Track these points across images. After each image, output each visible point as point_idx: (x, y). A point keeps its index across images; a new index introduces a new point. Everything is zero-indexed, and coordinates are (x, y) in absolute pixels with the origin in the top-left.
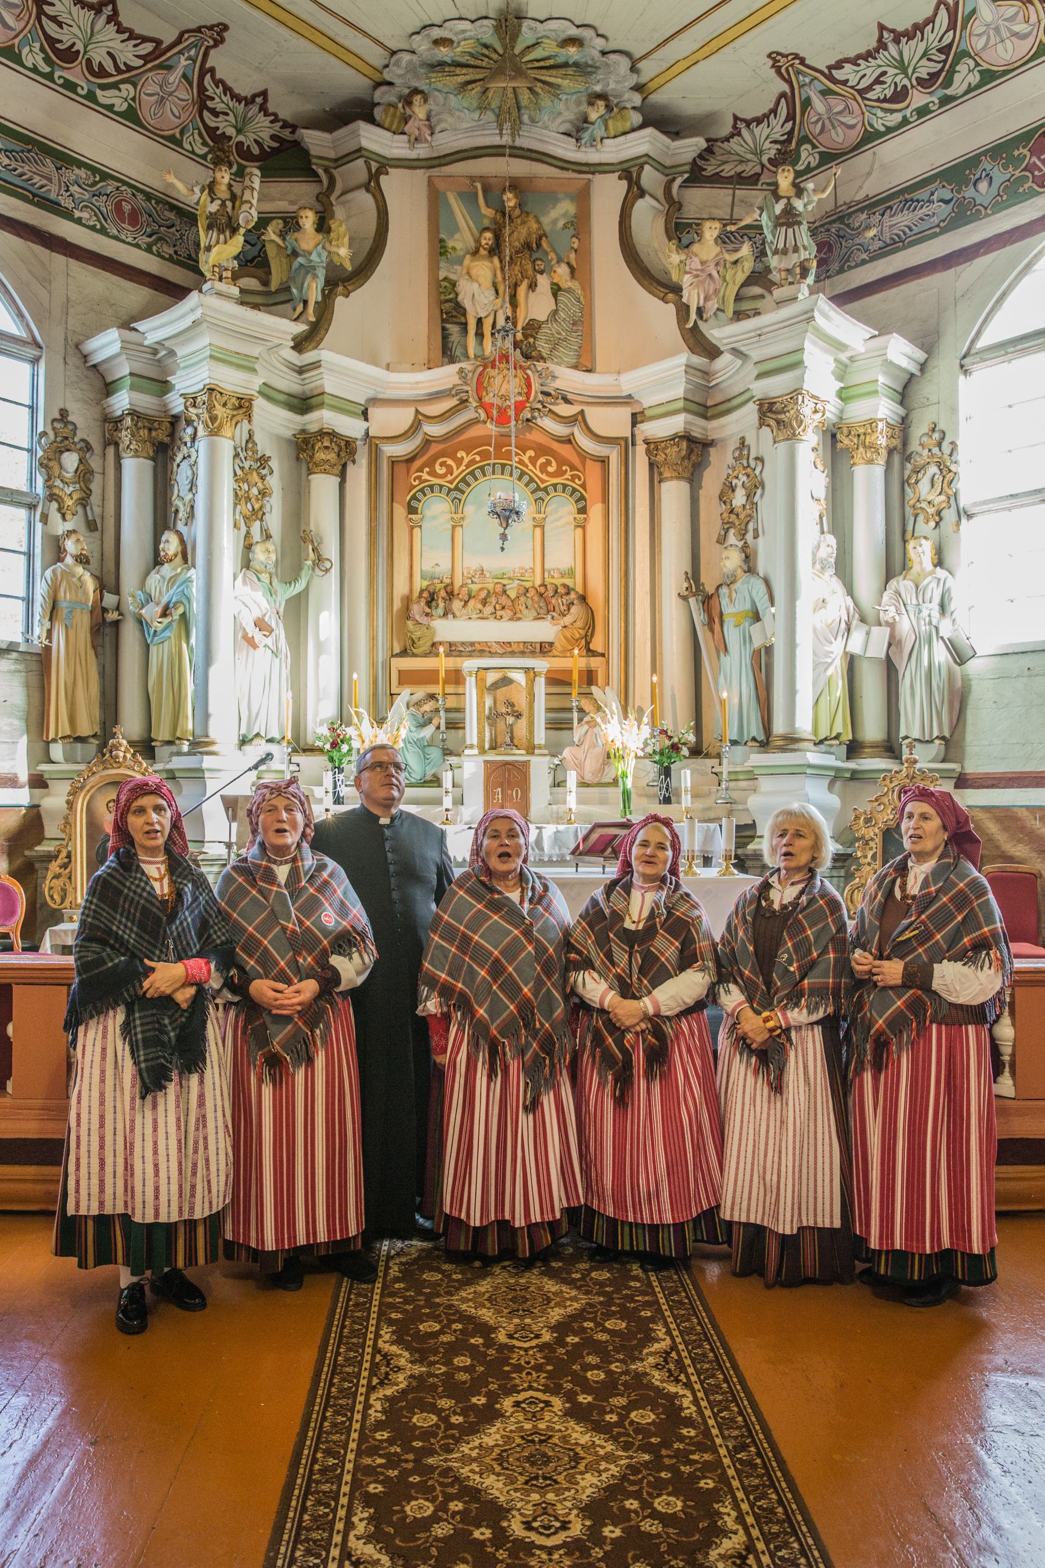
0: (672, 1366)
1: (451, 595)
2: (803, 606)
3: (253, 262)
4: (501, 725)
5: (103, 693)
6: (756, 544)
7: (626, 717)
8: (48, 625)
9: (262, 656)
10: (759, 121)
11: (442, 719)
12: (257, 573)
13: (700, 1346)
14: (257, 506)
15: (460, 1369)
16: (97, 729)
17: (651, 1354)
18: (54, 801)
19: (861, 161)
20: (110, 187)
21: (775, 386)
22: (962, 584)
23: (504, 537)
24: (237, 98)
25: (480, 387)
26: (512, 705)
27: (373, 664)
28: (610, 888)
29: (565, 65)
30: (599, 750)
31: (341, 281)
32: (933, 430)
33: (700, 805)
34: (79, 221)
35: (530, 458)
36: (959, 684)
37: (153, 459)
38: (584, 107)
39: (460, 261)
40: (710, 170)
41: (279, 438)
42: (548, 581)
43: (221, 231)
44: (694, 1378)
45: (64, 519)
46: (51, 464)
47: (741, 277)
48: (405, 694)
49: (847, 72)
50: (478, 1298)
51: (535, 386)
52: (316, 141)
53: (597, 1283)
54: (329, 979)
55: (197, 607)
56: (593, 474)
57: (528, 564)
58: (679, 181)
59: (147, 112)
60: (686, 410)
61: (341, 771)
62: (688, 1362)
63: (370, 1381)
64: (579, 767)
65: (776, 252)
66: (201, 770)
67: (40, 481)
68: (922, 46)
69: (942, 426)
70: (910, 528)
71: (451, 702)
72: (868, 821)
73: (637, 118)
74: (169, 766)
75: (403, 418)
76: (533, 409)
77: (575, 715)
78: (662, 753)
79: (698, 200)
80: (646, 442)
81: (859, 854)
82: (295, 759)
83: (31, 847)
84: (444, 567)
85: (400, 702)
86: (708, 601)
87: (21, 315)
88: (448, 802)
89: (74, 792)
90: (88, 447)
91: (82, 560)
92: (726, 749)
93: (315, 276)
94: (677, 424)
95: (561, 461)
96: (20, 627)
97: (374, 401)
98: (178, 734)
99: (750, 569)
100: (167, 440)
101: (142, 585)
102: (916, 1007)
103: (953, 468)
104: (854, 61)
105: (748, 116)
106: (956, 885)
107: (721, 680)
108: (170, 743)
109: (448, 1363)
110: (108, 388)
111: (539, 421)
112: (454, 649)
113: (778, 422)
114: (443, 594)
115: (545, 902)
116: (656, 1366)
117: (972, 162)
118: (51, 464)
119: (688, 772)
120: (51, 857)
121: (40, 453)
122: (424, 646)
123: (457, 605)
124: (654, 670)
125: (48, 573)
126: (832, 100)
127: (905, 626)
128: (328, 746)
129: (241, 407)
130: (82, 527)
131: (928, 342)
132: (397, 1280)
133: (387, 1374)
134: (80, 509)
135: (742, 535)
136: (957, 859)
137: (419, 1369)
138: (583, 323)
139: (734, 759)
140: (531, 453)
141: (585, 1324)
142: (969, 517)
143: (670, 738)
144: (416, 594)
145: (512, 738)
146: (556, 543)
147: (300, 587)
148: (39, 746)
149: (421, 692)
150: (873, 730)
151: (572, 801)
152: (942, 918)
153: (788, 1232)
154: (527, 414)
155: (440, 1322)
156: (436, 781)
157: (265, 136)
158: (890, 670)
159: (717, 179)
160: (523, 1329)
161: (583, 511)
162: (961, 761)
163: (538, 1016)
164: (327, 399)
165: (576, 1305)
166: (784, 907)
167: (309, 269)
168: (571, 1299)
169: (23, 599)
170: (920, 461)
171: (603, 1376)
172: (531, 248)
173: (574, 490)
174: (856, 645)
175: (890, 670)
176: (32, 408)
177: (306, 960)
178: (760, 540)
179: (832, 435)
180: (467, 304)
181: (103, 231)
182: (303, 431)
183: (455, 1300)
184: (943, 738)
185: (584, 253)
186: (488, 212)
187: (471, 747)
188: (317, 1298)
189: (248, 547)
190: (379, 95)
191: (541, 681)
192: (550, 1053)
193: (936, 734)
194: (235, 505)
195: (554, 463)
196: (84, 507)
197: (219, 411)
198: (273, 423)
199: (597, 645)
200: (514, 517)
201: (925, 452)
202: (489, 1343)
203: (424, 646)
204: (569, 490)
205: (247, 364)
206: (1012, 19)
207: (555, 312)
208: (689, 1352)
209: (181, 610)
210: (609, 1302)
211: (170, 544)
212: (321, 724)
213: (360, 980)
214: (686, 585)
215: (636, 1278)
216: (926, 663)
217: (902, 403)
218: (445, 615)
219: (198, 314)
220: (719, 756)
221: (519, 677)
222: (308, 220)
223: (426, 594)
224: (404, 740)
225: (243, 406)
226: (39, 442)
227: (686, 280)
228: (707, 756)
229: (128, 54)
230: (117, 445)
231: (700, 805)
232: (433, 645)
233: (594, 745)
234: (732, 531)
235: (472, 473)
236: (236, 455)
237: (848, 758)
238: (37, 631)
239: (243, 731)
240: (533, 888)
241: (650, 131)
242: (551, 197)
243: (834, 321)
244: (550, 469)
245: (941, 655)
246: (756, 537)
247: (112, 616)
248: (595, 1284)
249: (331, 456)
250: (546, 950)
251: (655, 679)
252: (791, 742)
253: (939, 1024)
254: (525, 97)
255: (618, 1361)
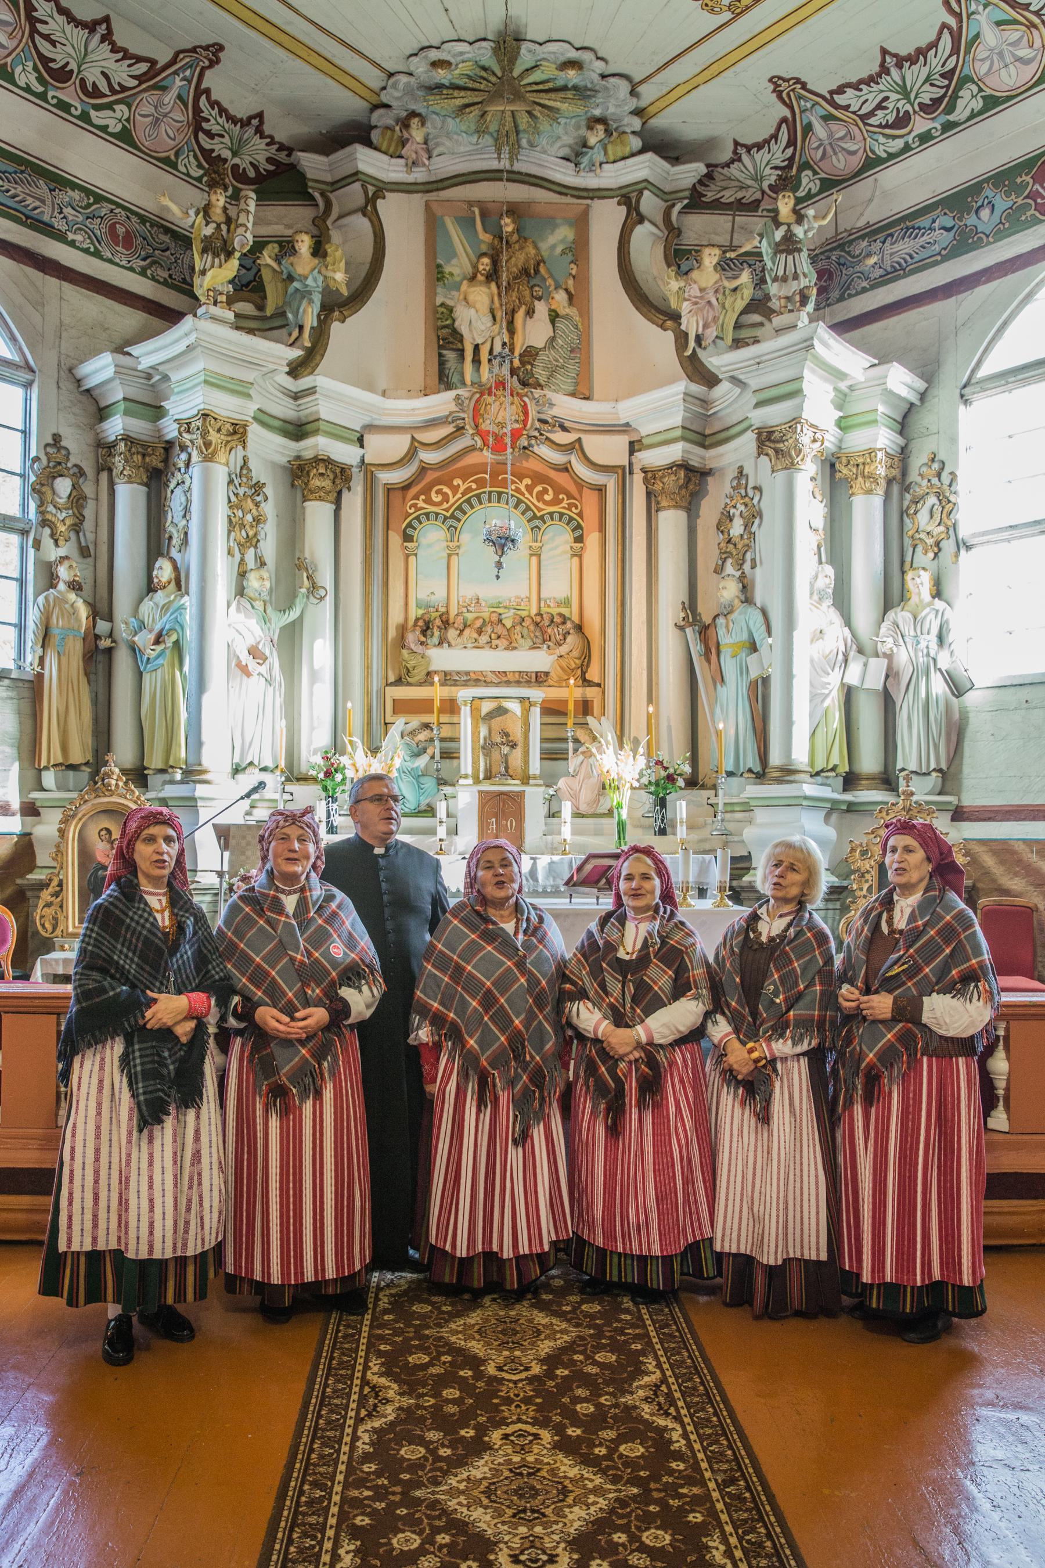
0: (662, 1399)
1: (446, 624)
2: (800, 637)
3: (249, 286)
4: (496, 755)
5: (96, 720)
6: (754, 575)
7: (621, 747)
8: (40, 652)
9: (255, 685)
10: (759, 146)
11: (436, 748)
12: (251, 600)
13: (691, 1380)
14: (251, 533)
15: (448, 1401)
16: (89, 757)
17: (640, 1387)
18: (46, 829)
19: (862, 189)
20: (104, 209)
21: (773, 415)
22: (961, 615)
23: (499, 565)
24: (232, 119)
25: (476, 414)
26: (507, 735)
27: (368, 693)
28: (604, 920)
29: (564, 88)
30: (594, 780)
31: (338, 305)
32: (933, 460)
33: (695, 836)
34: (72, 244)
35: (527, 486)
36: (957, 716)
37: (146, 485)
38: (583, 131)
39: (457, 287)
40: (710, 196)
41: (274, 465)
42: (544, 610)
43: (216, 255)
44: (684, 1412)
45: (57, 545)
46: (44, 489)
47: (740, 305)
48: (399, 724)
49: (848, 98)
50: (468, 1331)
51: (532, 413)
52: (312, 164)
53: (587, 1315)
54: (340, 1010)
55: (190, 634)
56: (589, 503)
57: (524, 593)
58: (678, 207)
59: (140, 135)
60: (683, 438)
61: (335, 800)
62: (677, 1395)
63: (358, 1413)
64: (575, 798)
65: (775, 279)
66: (194, 799)
67: (32, 506)
68: (925, 72)
69: (941, 456)
70: (908, 559)
71: (446, 732)
72: (864, 853)
73: (636, 143)
74: (161, 795)
75: (399, 445)
76: (529, 437)
77: (571, 745)
78: (657, 784)
79: (697, 226)
80: (644, 471)
81: (855, 887)
82: (289, 788)
83: (22, 876)
84: (440, 596)
85: (394, 731)
86: (705, 631)
87: (13, 339)
88: (442, 832)
89: (66, 821)
90: (81, 473)
91: (75, 586)
92: (722, 780)
93: (311, 301)
94: (675, 452)
95: (558, 490)
96: (13, 654)
97: (370, 428)
98: (171, 763)
99: (748, 599)
100: (161, 466)
101: (135, 612)
102: (906, 1039)
103: (952, 498)
104: (856, 86)
105: (749, 142)
106: (943, 918)
107: (718, 711)
108: (163, 771)
109: (437, 1395)
110: (102, 413)
111: (536, 449)
112: (448, 679)
113: (777, 451)
114: (438, 622)
115: (539, 934)
116: (646, 1399)
117: (975, 189)
118: (44, 489)
119: (684, 803)
120: (42, 886)
121: (33, 478)
122: (419, 675)
123: (452, 634)
124: (650, 700)
125: (41, 599)
126: (834, 126)
127: (902, 657)
128: (321, 776)
129: (235, 433)
130: (75, 554)
131: (928, 372)
132: (386, 1311)
133: (375, 1406)
134: (72, 535)
135: (740, 565)
136: (942, 891)
137: (408, 1401)
138: (581, 350)
139: (730, 791)
140: (527, 481)
141: (575, 1357)
142: (968, 548)
143: (666, 768)
144: (411, 623)
145: (507, 768)
146: (552, 572)
147: (294, 615)
148: (31, 774)
149: (415, 722)
150: (869, 762)
151: (566, 832)
152: (930, 952)
153: (772, 1262)
154: (523, 442)
155: (429, 1354)
156: (430, 811)
157: (261, 158)
158: (888, 702)
159: (716, 206)
160: (513, 1361)
161: (579, 539)
162: (958, 794)
163: (529, 1047)
164: (322, 426)
165: (566, 1338)
166: (771, 939)
167: (305, 294)
168: (562, 1332)
169: (15, 625)
170: (919, 492)
171: (592, 1409)
172: (529, 273)
173: (571, 519)
174: (853, 677)
175: (888, 702)
176: (24, 432)
177: (315, 992)
178: (758, 570)
179: (831, 465)
180: (464, 330)
181: (97, 254)
182: (298, 458)
183: (444, 1332)
184: (940, 771)
185: (582, 279)
186: (485, 237)
187: (466, 777)
188: (304, 1334)
189: (242, 575)
190: (376, 117)
191: (536, 711)
192: (540, 1087)
193: (933, 766)
194: (229, 532)
195: (551, 492)
196: (78, 533)
197: (214, 437)
198: (268, 450)
199: (593, 675)
200: (510, 545)
201: (925, 483)
202: (479, 1375)
203: (419, 675)
204: (565, 518)
205: (241, 390)
206: (1015, 44)
207: (553, 339)
208: (679, 1385)
209: (174, 638)
210: (600, 1334)
211: (164, 571)
212: (315, 753)
213: (368, 1014)
214: (682, 615)
215: (627, 1311)
216: (923, 694)
217: (901, 433)
218: (440, 643)
219: (192, 339)
220: (714, 787)
221: (515, 707)
222: (304, 244)
223: (421, 623)
224: (398, 770)
225: (238, 432)
226: (32, 467)
227: (685, 307)
228: (703, 787)
229: (123, 74)
230: (110, 470)
231: (695, 836)
232: (428, 674)
233: (588, 776)
234: (729, 561)
235: (468, 501)
236: (231, 482)
237: (845, 790)
238: (29, 658)
239: (236, 760)
240: (528, 920)
241: (649, 156)
242: (550, 222)
243: (834, 350)
244: (547, 498)
245: (939, 687)
246: (753, 567)
247: (105, 643)
248: (585, 1317)
249: (326, 483)
250: (539, 982)
251: (651, 709)
252: (787, 773)
253: (930, 1057)
254: (524, 121)
255: (607, 1393)
